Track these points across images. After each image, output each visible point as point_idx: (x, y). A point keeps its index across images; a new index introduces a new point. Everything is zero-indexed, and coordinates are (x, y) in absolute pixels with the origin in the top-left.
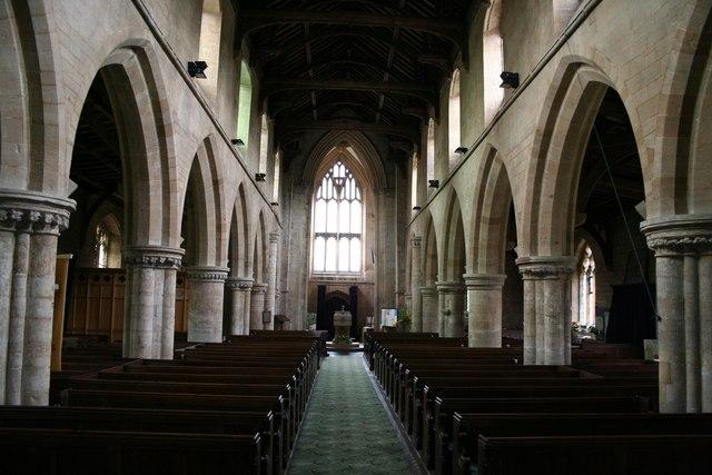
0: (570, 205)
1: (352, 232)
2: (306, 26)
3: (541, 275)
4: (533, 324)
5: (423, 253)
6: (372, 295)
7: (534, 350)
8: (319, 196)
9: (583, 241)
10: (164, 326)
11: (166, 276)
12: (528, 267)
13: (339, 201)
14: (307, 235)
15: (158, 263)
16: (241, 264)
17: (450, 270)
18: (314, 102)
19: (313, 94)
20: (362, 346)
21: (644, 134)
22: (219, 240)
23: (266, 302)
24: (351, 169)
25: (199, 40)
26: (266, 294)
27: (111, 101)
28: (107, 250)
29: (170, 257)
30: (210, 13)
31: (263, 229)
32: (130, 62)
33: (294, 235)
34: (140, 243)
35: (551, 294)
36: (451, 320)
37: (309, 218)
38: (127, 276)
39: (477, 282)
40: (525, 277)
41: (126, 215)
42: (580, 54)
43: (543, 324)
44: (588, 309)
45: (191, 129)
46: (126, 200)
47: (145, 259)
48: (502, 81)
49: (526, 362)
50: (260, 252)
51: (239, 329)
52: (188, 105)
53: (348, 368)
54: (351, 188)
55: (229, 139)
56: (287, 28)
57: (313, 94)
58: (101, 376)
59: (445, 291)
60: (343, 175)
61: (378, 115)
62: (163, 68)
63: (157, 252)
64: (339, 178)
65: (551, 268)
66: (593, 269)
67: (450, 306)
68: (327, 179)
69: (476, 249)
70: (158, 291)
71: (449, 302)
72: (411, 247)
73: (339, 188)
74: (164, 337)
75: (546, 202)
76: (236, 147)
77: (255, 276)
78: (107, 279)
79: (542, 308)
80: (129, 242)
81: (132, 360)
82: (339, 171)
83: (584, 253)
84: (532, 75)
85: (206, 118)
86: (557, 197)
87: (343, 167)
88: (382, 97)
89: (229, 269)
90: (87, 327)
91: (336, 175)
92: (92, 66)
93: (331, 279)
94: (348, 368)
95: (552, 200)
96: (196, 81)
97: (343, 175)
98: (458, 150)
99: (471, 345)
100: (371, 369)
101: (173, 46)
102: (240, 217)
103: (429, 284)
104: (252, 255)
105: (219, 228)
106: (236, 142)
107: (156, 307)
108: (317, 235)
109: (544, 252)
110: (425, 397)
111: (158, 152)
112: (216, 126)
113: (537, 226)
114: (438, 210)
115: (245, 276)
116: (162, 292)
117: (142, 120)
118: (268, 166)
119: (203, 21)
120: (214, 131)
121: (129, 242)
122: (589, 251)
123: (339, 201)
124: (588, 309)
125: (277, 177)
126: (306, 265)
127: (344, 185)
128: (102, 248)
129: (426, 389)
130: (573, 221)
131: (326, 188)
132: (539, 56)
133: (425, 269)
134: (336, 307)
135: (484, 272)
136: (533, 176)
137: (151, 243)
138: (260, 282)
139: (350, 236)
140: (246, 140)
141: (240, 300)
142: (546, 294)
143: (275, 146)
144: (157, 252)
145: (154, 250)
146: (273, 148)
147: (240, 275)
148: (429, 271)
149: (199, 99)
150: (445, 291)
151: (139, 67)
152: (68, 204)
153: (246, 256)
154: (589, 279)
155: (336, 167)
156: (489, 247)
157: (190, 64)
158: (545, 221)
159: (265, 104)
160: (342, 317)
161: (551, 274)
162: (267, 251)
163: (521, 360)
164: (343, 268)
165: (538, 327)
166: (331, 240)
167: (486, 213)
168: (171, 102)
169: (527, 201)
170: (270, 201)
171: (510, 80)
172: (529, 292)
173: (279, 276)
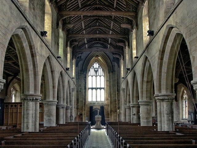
0: (172, 76)
1: (101, 87)
2: (82, 16)
3: (163, 100)
4: (161, 117)
5: (125, 94)
6: (108, 109)
7: (161, 126)
8: (89, 75)
9: (183, 88)
10: (36, 121)
11: (36, 104)
12: (158, 97)
13: (96, 76)
14: (85, 88)
15: (33, 99)
16: (62, 99)
17: (135, 99)
18: (86, 42)
19: (85, 39)
20: (105, 127)
21: (192, 51)
22: (54, 91)
23: (71, 112)
24: (101, 65)
25: (44, 24)
26: (71, 110)
27: (14, 42)
28: (15, 96)
29: (37, 97)
30: (48, 14)
31: (69, 87)
32: (21, 32)
33: (81, 89)
34: (26, 93)
35: (166, 106)
36: (135, 117)
37: (86, 83)
38: (22, 105)
39: (143, 103)
40: (157, 101)
41: (22, 84)
42: (172, 24)
43: (164, 117)
44: (186, 112)
45: (43, 54)
46: (21, 79)
47: (29, 98)
48: (148, 34)
49: (159, 130)
50: (68, 95)
51: (62, 122)
52: (41, 46)
53: (99, 133)
54: (100, 71)
55: (56, 56)
56: (74, 17)
57: (85, 39)
58: (14, 137)
59: (133, 107)
60: (97, 67)
61: (109, 45)
62: (33, 34)
63: (32, 96)
64: (96, 68)
65: (166, 98)
66: (187, 98)
67: (135, 112)
68: (92, 69)
69: (142, 92)
70: (32, 108)
71: (134, 111)
72: (121, 92)
73: (96, 72)
74: (35, 124)
75: (164, 75)
76: (59, 59)
77: (67, 103)
78: (16, 106)
79: (163, 111)
80: (23, 93)
81: (25, 132)
82: (96, 65)
83: (183, 92)
84: (157, 31)
85: (47, 46)
86: (168, 72)
87: (97, 64)
88: (110, 39)
89: (57, 101)
90: (9, 123)
91: (95, 67)
92: (9, 36)
93: (95, 104)
94: (99, 133)
95: (166, 74)
96: (43, 38)
97: (97, 67)
98: (135, 57)
99: (141, 125)
100: (108, 135)
101: (35, 27)
102: (61, 83)
103: (128, 105)
104: (65, 98)
105: (54, 87)
106: (58, 57)
107: (32, 114)
108: (89, 88)
109: (164, 92)
110: (123, 144)
111: (32, 62)
112: (51, 53)
113: (161, 84)
114: (130, 78)
115: (63, 103)
116: (34, 109)
117: (26, 52)
118: (70, 65)
119: (45, 16)
120: (51, 54)
121: (23, 93)
122: (185, 92)
123: (96, 76)
124: (186, 112)
125: (74, 69)
126: (85, 99)
127: (98, 70)
128: (13, 95)
129: (121, 138)
130: (174, 81)
131: (92, 72)
132: (161, 23)
133: (126, 99)
134: (94, 114)
135: (145, 100)
136: (159, 66)
137: (30, 93)
138: (69, 105)
139: (100, 89)
140: (62, 57)
141: (62, 112)
142: (165, 106)
143: (73, 58)
144: (32, 96)
145: (32, 95)
146: (72, 58)
147: (62, 103)
148: (128, 100)
149: (45, 44)
150: (133, 107)
151: (24, 35)
152: (3, 81)
153: (64, 96)
154: (186, 102)
155: (95, 64)
156: (147, 91)
157: (41, 32)
158: (164, 82)
159: (69, 43)
160: (98, 117)
161: (166, 99)
162: (71, 95)
163: (157, 130)
164: (99, 100)
165: (162, 118)
166: (99, 90)
167: (145, 79)
168: (35, 46)
169: (157, 74)
170: (72, 77)
171: (151, 33)
172: (159, 106)
173: (76, 104)
